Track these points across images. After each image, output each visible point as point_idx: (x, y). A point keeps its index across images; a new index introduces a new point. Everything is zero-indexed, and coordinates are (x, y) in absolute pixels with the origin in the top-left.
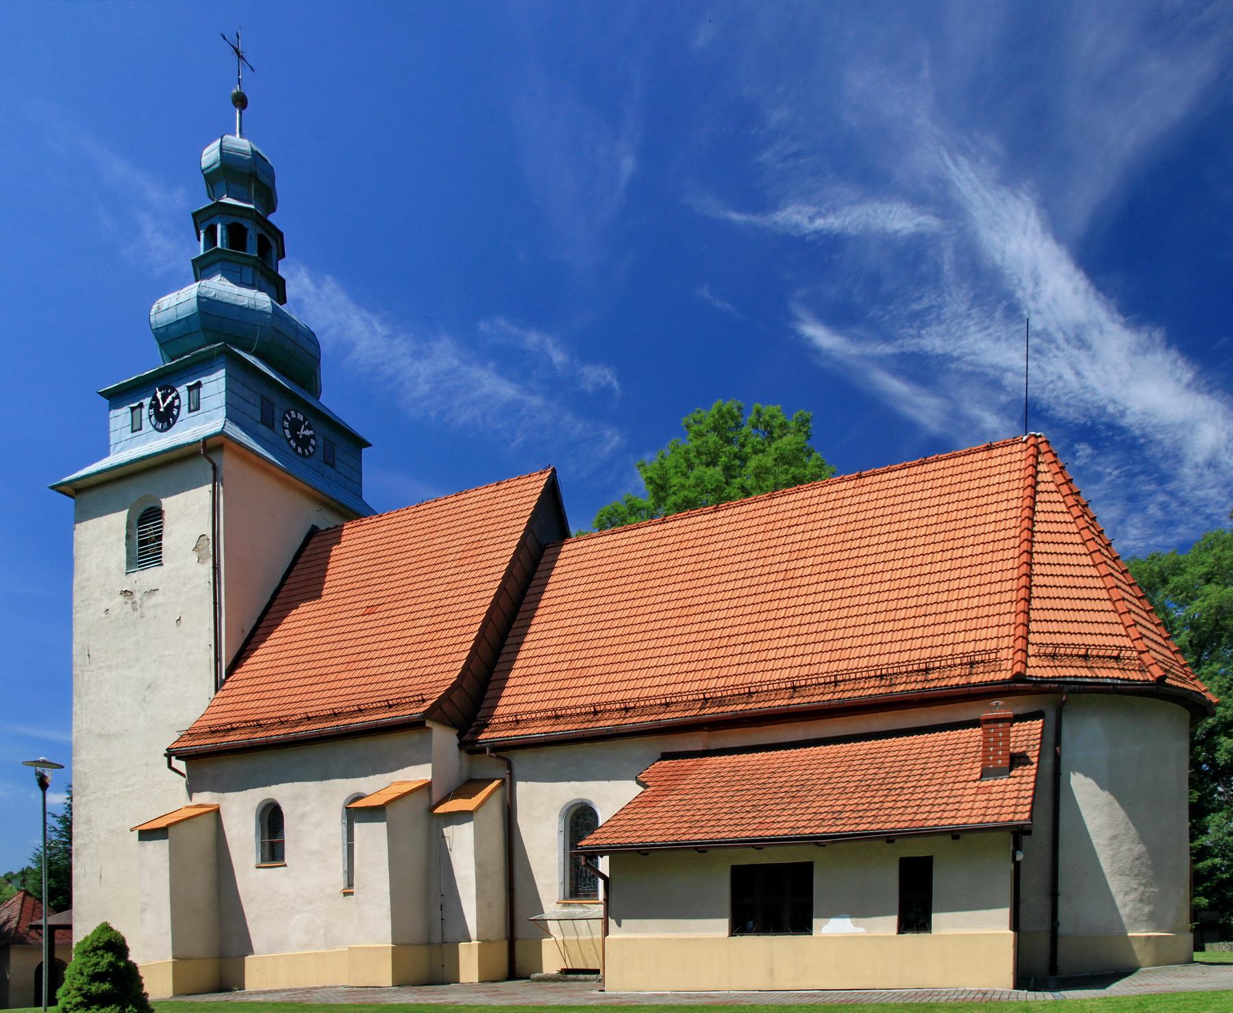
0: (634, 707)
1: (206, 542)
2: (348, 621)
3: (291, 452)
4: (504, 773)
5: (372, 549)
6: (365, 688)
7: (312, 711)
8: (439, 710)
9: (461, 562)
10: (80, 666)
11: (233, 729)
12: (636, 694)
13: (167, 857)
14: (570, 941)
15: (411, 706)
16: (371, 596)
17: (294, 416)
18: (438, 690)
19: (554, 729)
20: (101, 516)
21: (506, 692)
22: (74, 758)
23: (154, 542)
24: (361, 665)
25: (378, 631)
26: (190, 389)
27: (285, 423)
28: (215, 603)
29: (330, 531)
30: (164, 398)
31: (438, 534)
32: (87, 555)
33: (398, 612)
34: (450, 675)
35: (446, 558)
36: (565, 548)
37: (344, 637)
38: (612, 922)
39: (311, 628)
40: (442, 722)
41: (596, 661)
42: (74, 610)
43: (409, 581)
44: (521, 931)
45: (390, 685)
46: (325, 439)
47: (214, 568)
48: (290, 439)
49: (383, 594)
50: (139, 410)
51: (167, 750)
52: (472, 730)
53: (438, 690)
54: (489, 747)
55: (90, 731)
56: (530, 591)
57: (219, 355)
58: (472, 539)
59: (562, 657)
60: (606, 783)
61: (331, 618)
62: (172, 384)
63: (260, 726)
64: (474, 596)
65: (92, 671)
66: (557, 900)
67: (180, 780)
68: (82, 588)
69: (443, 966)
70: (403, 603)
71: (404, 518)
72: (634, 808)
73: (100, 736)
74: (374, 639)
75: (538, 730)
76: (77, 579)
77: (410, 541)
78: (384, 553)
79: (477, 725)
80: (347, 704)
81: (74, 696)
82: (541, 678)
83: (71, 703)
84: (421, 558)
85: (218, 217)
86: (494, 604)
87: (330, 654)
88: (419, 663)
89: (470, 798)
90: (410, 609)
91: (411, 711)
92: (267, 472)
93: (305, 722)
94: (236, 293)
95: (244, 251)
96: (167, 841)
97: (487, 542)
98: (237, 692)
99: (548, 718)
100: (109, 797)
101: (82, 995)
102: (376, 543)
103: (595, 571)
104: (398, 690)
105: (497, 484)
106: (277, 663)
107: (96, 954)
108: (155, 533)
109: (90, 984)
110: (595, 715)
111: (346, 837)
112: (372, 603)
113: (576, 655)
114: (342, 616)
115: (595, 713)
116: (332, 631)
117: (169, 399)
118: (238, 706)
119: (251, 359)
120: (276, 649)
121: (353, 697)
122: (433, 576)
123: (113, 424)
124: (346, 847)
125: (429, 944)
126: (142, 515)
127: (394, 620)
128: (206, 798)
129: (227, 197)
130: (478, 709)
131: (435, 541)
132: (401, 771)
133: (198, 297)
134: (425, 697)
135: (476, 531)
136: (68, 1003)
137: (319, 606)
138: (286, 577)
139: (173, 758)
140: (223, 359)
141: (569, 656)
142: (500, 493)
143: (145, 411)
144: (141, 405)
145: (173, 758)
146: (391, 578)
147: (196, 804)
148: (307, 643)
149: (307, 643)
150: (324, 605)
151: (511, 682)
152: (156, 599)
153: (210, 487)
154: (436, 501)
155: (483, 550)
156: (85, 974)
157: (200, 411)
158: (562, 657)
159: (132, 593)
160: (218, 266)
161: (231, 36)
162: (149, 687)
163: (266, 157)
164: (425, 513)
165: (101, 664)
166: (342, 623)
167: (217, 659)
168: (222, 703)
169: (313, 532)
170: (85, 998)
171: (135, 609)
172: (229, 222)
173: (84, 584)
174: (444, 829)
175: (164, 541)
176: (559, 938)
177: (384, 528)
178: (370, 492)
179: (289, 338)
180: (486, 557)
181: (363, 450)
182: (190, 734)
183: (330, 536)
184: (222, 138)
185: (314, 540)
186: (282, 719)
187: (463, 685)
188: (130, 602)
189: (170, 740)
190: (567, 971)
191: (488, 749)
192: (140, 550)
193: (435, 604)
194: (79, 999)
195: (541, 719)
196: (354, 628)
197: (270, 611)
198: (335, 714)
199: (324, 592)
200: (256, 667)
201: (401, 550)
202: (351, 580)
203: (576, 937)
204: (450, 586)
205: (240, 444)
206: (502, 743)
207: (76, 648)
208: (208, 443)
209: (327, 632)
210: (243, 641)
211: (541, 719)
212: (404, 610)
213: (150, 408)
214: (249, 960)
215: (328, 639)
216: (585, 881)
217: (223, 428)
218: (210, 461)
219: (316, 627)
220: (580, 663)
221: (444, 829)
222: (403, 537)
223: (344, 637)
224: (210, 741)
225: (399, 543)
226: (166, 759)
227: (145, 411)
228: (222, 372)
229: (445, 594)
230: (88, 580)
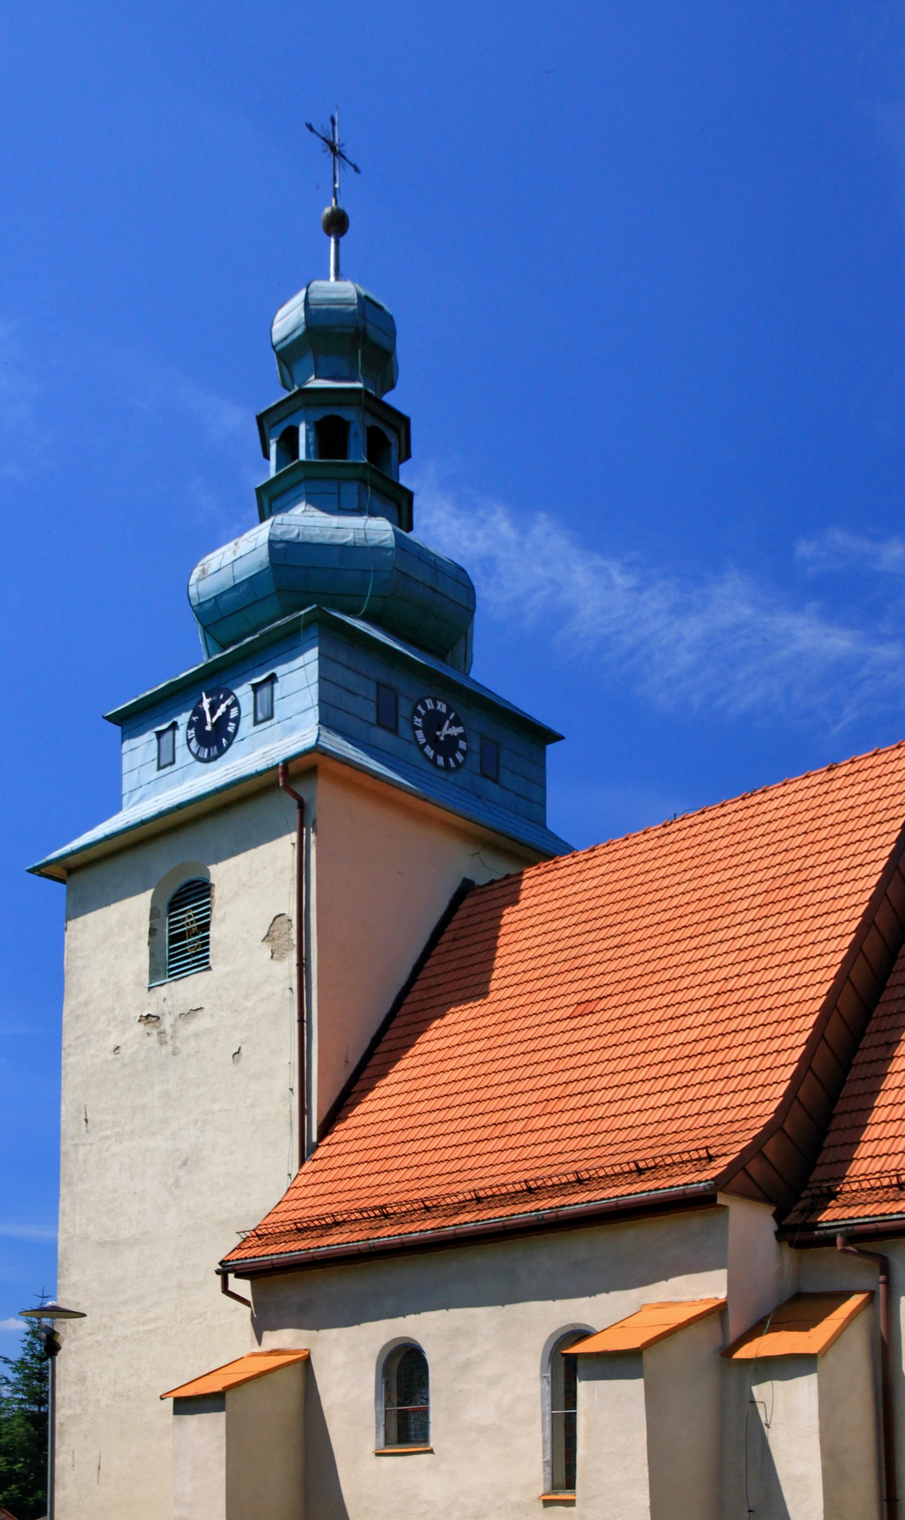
1: (286, 926)
2: (541, 1031)
3: (428, 766)
6: (585, 1142)
9: (765, 911)
10: (72, 1139)
15: (685, 1169)
16: (585, 984)
20: (108, 904)
21: (871, 1133)
22: (59, 1281)
24: (573, 1102)
25: (603, 1042)
26: (256, 687)
28: (301, 1021)
29: (496, 885)
30: (213, 709)
31: (711, 868)
33: (641, 1007)
34: (759, 1110)
37: (536, 1057)
39: (470, 1048)
40: (745, 1194)
42: (63, 1053)
45: (635, 1134)
46: (483, 738)
47: (300, 965)
48: (424, 745)
49: (607, 979)
50: (170, 733)
51: (221, 1263)
52: (801, 1205)
54: (842, 1234)
55: (87, 1238)
57: (307, 625)
58: (784, 869)
61: (508, 1027)
62: (226, 686)
65: (91, 1144)
68: (77, 1018)
73: (102, 1244)
74: (595, 1057)
76: (69, 1005)
77: (655, 885)
78: (605, 911)
79: (814, 1196)
80: (550, 1171)
81: (62, 1185)
83: (57, 1196)
85: (301, 413)
86: (842, 978)
92: (386, 801)
93: (473, 1206)
94: (335, 525)
96: (222, 1416)
98: (339, 1161)
100: (116, 1341)
102: (588, 895)
104: (651, 1142)
106: (410, 1110)
108: (197, 920)
111: (548, 1401)
112: (587, 996)
114: (528, 1022)
117: (222, 708)
119: (360, 625)
120: (407, 1086)
121: (562, 1158)
122: (707, 939)
123: (127, 762)
124: (548, 1418)
127: (633, 1021)
129: (317, 378)
130: (811, 1166)
131: (706, 881)
132: (663, 1284)
133: (271, 543)
134: (712, 1152)
135: (791, 855)
137: (483, 1010)
138: (418, 967)
139: (231, 1276)
140: (314, 631)
142: (838, 784)
143: (181, 735)
144: (174, 726)
145: (231, 1276)
146: (621, 952)
147: (269, 1348)
149: (464, 1073)
153: (294, 837)
154: (703, 813)
155: (811, 886)
157: (274, 721)
159: (158, 1018)
160: (302, 489)
163: (382, 303)
165: (107, 1133)
166: (531, 1033)
167: (304, 1111)
168: (313, 1180)
169: (466, 889)
171: (163, 1043)
174: (755, 1389)
177: (602, 870)
179: (424, 584)
180: (818, 896)
182: (259, 1235)
184: (308, 287)
185: (469, 902)
186: (427, 1203)
187: (786, 1126)
188: (155, 1032)
191: (839, 1240)
192: (171, 950)
193: (716, 988)
196: (555, 1040)
197: (394, 1024)
199: (493, 985)
200: (372, 1118)
201: (637, 901)
202: (543, 961)
206: (872, 1226)
207: (66, 1110)
208: (292, 768)
210: (348, 1076)
213: (189, 728)
215: (505, 1064)
217: (318, 740)
219: (480, 1045)
221: (755, 1389)
223: (536, 1057)
224: (296, 1247)
226: (219, 1278)
227: (181, 735)
230: (86, 1004)
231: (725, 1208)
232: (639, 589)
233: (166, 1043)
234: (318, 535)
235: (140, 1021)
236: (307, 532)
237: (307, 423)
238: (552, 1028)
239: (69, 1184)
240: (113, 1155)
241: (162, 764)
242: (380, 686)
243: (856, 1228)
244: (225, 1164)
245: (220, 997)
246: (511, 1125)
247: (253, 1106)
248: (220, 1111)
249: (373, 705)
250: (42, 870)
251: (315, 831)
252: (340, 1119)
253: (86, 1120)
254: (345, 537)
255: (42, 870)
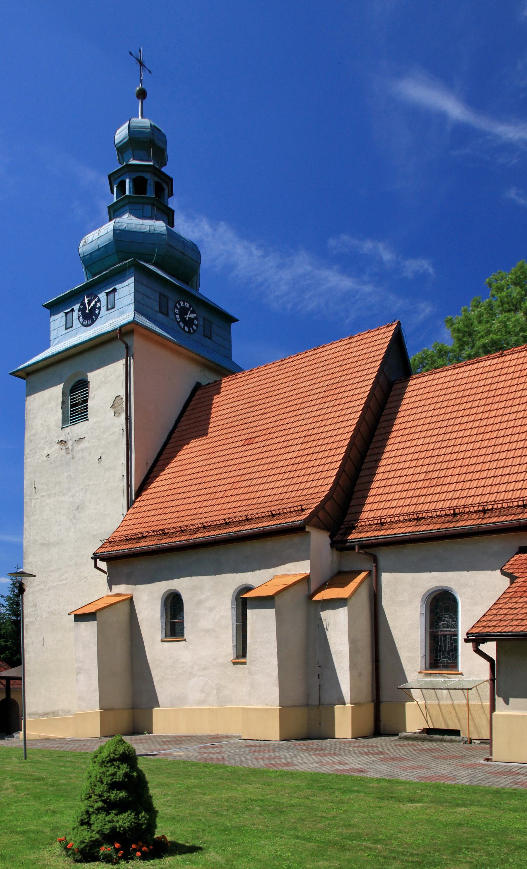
0: (492, 509)
1: (121, 401)
3: (181, 331)
4: (370, 565)
5: (247, 396)
6: (249, 502)
7: (206, 520)
8: (315, 518)
10: (29, 496)
11: (143, 537)
12: (493, 498)
13: (96, 634)
14: (432, 705)
17: (182, 304)
18: (314, 501)
19: (417, 529)
20: (44, 390)
22: (24, 561)
23: (82, 404)
26: (107, 294)
27: (176, 310)
28: (127, 444)
30: (89, 303)
32: (34, 418)
33: (273, 441)
34: (323, 489)
35: (311, 398)
36: (411, 382)
38: (499, 701)
39: (200, 458)
40: (318, 527)
41: (450, 472)
43: (280, 417)
44: (385, 696)
45: (271, 498)
46: (205, 319)
48: (179, 322)
49: (258, 429)
50: (71, 313)
51: (93, 554)
52: (341, 532)
53: (314, 501)
55: (36, 542)
56: (383, 418)
57: (130, 267)
58: (332, 381)
59: (418, 470)
60: (465, 573)
63: (165, 534)
64: (338, 426)
65: (37, 499)
66: (419, 670)
67: (100, 575)
68: (31, 441)
69: (320, 724)
70: (276, 435)
71: (271, 370)
72: (511, 598)
73: (42, 544)
74: (254, 463)
75: (403, 530)
76: (27, 435)
77: (278, 387)
79: (346, 528)
82: (400, 488)
84: (289, 399)
87: (217, 477)
88: (294, 481)
89: (343, 587)
90: (283, 439)
91: (293, 519)
94: (141, 223)
95: (146, 194)
97: (346, 383)
98: (144, 509)
99: (410, 520)
100: (49, 588)
101: (102, 801)
103: (441, 399)
104: (278, 503)
105: (350, 338)
106: (175, 486)
107: (113, 765)
108: (83, 398)
109: (109, 792)
110: (454, 516)
113: (431, 468)
115: (455, 515)
116: (218, 459)
117: (93, 303)
118: (146, 520)
119: (152, 268)
120: (173, 475)
121: (240, 509)
122: (300, 412)
124: (235, 626)
125: (308, 705)
126: (73, 387)
127: (270, 448)
128: (122, 589)
129: (133, 160)
133: (114, 230)
134: (303, 507)
136: (90, 806)
137: (206, 441)
139: (98, 560)
140: (132, 270)
141: (425, 469)
142: (353, 345)
144: (73, 310)
146: (264, 416)
147: (115, 593)
148: (198, 470)
150: (209, 441)
151: (372, 492)
152: (84, 444)
153: (124, 361)
156: (105, 782)
157: (115, 309)
158: (418, 470)
160: (127, 207)
161: (135, 52)
162: (78, 509)
163: (161, 129)
164: (289, 365)
167: (129, 486)
169: (198, 387)
170: (104, 804)
171: (68, 453)
172: (134, 177)
173: (32, 438)
174: (321, 613)
175: (90, 403)
176: (422, 702)
177: (256, 380)
178: (237, 356)
181: (232, 324)
182: (110, 542)
183: (211, 389)
184: (130, 121)
185: (199, 392)
188: (64, 448)
189: (95, 546)
190: (428, 731)
191: (356, 547)
192: (71, 411)
193: (304, 434)
194: (100, 804)
195: (404, 521)
196: (236, 456)
198: (226, 523)
199: (210, 430)
200: (159, 489)
201: (271, 394)
202: (231, 420)
203: (437, 702)
204: (316, 419)
205: (146, 328)
206: (370, 541)
207: (26, 483)
208: (123, 330)
209: (214, 461)
211: (404, 521)
212: (278, 440)
213: (79, 311)
214: (155, 710)
216: (443, 654)
217: (134, 318)
218: (125, 343)
220: (435, 474)
221: (321, 613)
222: (272, 384)
223: (228, 463)
224: (126, 547)
225: (269, 390)
226: (93, 561)
227: (75, 314)
228: (132, 279)
229: (312, 426)
231: (309, 532)
232: (264, 257)
233: (69, 453)
234: (134, 228)
235: (58, 443)
236: (129, 226)
237: (129, 179)
238: (235, 450)
239: (28, 517)
240: (47, 504)
241: (67, 327)
242: (161, 295)
243: (364, 542)
244: (95, 509)
245: (92, 433)
246: (218, 494)
247: (107, 483)
248: (93, 485)
249: (158, 303)
250: (16, 374)
251: (133, 358)
252: (144, 489)
253: (35, 488)
254: (145, 229)
255: (16, 374)
